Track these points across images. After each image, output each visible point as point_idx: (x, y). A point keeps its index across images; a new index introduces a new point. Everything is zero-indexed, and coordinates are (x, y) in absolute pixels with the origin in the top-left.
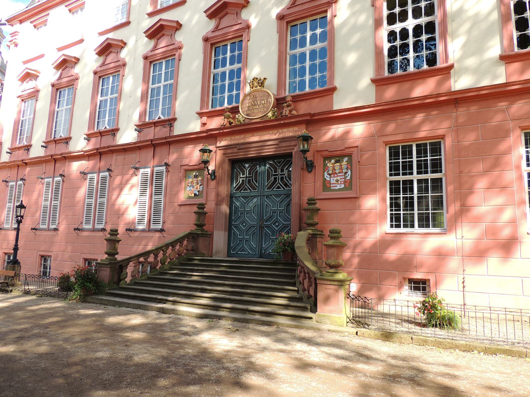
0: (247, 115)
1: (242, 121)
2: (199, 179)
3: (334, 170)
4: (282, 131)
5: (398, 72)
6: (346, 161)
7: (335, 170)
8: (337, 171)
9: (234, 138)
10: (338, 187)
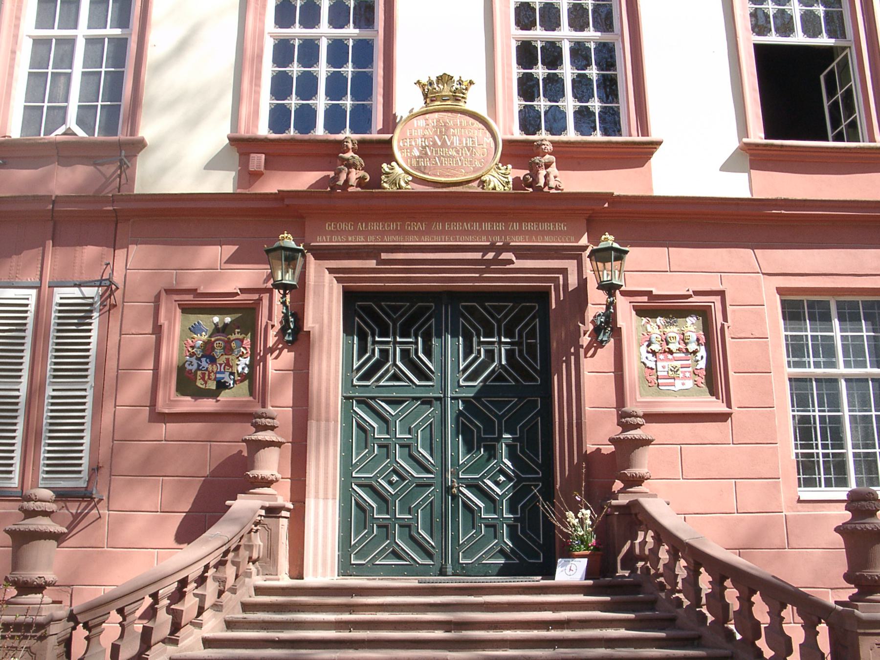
0: (418, 169)
1: (403, 184)
2: (233, 337)
3: (664, 343)
4: (507, 227)
5: (290, 132)
7: (668, 343)
8: (673, 347)
9: (366, 226)
10: (678, 385)
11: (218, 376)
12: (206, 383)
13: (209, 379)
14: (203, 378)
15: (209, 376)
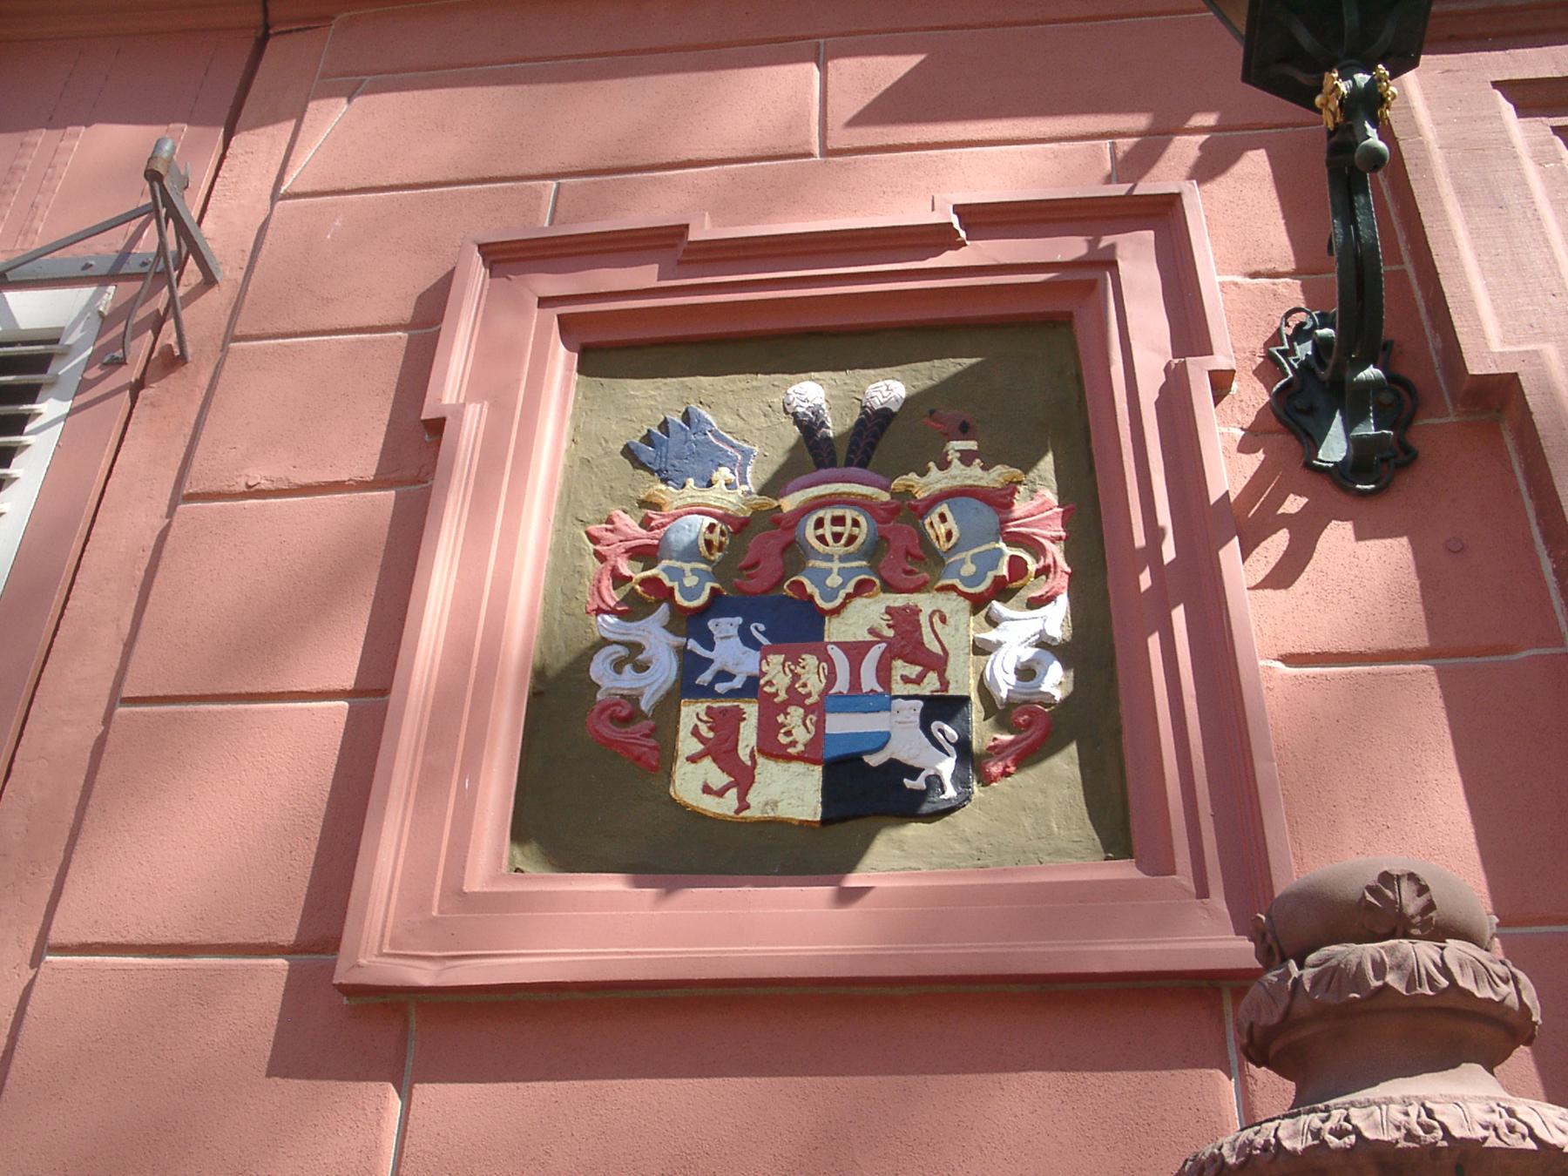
6: (923, 472)
11: (838, 724)
12: (743, 778)
13: (771, 748)
14: (721, 749)
15: (768, 728)
